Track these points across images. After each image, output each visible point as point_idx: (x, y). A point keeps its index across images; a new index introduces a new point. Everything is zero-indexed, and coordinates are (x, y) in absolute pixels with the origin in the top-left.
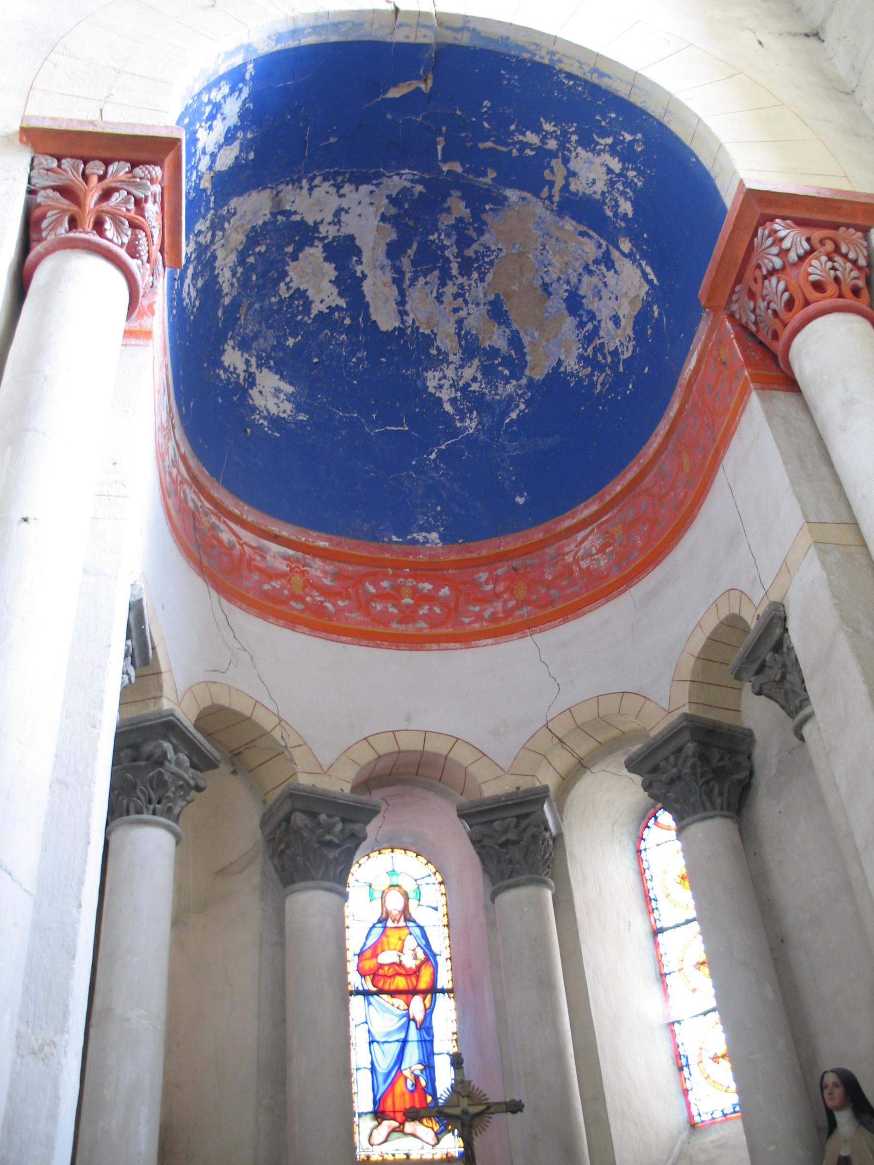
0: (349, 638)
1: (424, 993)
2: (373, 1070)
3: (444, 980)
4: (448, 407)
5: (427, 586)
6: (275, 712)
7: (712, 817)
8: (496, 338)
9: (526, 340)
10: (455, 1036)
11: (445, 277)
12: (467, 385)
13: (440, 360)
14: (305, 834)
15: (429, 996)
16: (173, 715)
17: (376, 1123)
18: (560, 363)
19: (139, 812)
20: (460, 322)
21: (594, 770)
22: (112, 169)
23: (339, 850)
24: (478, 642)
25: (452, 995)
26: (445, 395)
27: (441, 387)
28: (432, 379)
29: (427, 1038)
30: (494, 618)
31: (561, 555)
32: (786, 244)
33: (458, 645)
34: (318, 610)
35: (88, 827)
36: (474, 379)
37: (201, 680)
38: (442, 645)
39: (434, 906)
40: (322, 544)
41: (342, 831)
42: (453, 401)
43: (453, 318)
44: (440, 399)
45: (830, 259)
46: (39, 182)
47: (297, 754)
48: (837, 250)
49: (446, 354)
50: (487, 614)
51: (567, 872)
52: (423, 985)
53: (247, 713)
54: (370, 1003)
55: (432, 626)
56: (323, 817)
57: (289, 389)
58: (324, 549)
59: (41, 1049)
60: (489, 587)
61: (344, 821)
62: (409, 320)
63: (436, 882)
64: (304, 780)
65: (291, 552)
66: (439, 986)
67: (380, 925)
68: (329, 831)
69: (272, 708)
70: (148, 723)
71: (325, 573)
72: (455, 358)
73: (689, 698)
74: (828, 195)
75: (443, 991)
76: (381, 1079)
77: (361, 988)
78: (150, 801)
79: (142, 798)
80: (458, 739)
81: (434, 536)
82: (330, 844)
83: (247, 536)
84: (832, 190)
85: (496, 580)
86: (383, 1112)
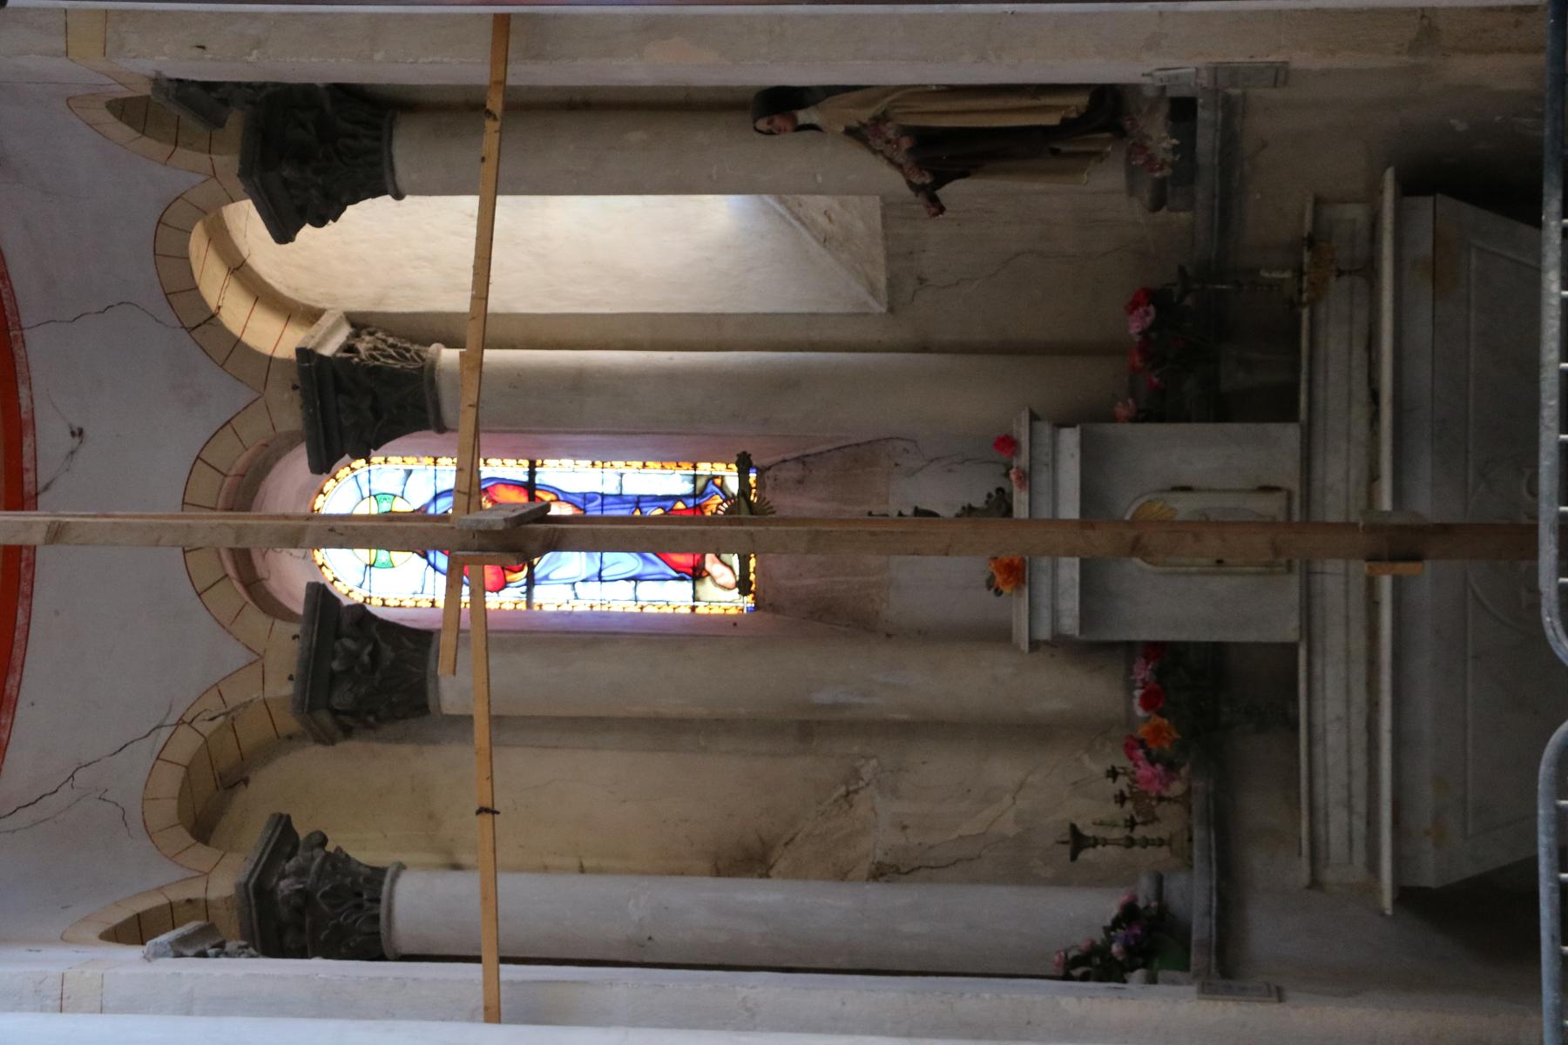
0: (20, 611)
2: (636, 579)
6: (170, 730)
7: (391, 157)
10: (598, 463)
14: (363, 690)
15: (538, 494)
16: (246, 884)
17: (708, 579)
19: (376, 918)
21: (245, 254)
23: (383, 645)
24: (23, 410)
25: (539, 462)
29: (599, 501)
33: (27, 441)
35: (524, 982)
37: (149, 842)
38: (27, 463)
39: (403, 474)
41: (355, 639)
47: (235, 697)
51: (404, 315)
53: (180, 773)
54: (546, 578)
56: (335, 665)
59: (747, 1010)
61: (338, 637)
63: (367, 468)
64: (282, 689)
66: (525, 478)
67: (431, 556)
68: (353, 656)
69: (165, 733)
70: (254, 915)
73: (201, 151)
75: (532, 474)
76: (650, 569)
77: (524, 589)
78: (359, 907)
79: (354, 917)
80: (198, 457)
82: (374, 655)
86: (694, 568)
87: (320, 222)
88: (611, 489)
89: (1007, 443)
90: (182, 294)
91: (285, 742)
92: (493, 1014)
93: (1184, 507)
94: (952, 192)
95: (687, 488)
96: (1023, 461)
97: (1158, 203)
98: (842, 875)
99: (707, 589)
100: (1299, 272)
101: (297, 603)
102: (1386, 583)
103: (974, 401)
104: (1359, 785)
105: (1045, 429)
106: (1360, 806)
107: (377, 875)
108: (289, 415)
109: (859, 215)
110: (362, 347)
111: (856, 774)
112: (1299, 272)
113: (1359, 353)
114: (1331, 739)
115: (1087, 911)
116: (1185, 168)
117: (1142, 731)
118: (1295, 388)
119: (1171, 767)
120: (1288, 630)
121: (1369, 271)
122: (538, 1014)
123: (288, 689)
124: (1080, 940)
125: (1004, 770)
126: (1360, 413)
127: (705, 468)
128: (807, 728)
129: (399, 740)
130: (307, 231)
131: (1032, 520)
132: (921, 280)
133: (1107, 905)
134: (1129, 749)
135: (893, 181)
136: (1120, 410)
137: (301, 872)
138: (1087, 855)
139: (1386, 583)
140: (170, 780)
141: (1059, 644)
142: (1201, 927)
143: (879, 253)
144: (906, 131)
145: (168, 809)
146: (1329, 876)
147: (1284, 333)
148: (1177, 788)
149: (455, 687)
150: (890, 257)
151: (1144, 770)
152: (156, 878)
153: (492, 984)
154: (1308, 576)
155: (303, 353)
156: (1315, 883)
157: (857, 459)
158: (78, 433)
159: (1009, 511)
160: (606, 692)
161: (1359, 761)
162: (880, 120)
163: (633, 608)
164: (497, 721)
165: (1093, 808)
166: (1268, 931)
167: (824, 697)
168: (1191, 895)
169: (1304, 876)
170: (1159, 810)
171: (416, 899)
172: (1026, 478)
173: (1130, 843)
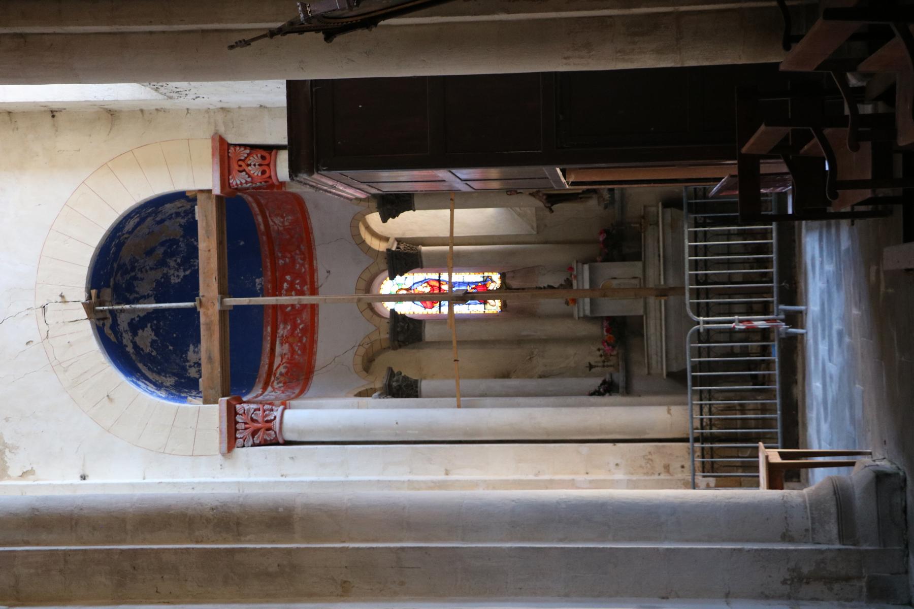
1: (440, 284)
3: (435, 276)
4: (188, 273)
5: (285, 285)
8: (160, 251)
9: (164, 239)
11: (135, 278)
12: (178, 264)
13: (166, 277)
18: (180, 225)
20: (151, 269)
22: (240, 421)
26: (182, 274)
27: (178, 276)
28: (174, 280)
30: (304, 259)
31: (278, 232)
32: (244, 181)
34: (304, 331)
36: (175, 261)
40: (269, 329)
42: (185, 270)
43: (149, 272)
44: (185, 276)
45: (250, 165)
46: (251, 442)
48: (243, 161)
49: (164, 274)
50: (301, 262)
52: (437, 285)
55: (306, 283)
57: (192, 347)
58: (272, 328)
60: (287, 260)
62: (151, 292)
65: (278, 343)
71: (284, 328)
72: (165, 270)
74: (217, 160)
81: (257, 280)
83: (277, 361)
84: (213, 155)
85: (284, 257)
87: (394, 217)
88: (461, 280)
89: (571, 269)
90: (357, 236)
91: (384, 350)
92: (459, 407)
93: (615, 282)
94: (555, 207)
95: (482, 279)
96: (575, 273)
97: (606, 207)
98: (531, 377)
99: (488, 306)
100: (641, 225)
101: (388, 315)
102: (663, 301)
103: (561, 256)
104: (659, 350)
105: (580, 264)
106: (659, 354)
107: (416, 382)
108: (383, 264)
109: (530, 211)
110: (402, 247)
111: (532, 353)
112: (641, 225)
113: (656, 244)
114: (652, 338)
115: (595, 382)
116: (612, 201)
117: (606, 338)
118: (640, 253)
119: (613, 347)
120: (641, 312)
121: (657, 224)
122: (467, 406)
123: (388, 336)
124: (592, 389)
125: (570, 351)
126: (657, 258)
127: (486, 274)
128: (519, 341)
129: (414, 348)
130: (391, 220)
131: (578, 289)
132: (546, 226)
133: (599, 381)
134: (603, 343)
135: (541, 204)
136: (598, 259)
137: (397, 381)
138: (593, 370)
139: (663, 301)
140: (359, 360)
141: (586, 318)
142: (622, 384)
143: (534, 219)
144: (544, 194)
145: (360, 367)
146: (652, 372)
147: (638, 238)
148: (615, 353)
149: (429, 333)
150: (537, 220)
151: (607, 348)
152: (363, 385)
153: (458, 401)
154: (645, 299)
155: (388, 250)
156: (649, 374)
157: (529, 271)
158: (328, 272)
159: (571, 285)
160: (471, 336)
161: (659, 344)
162: (538, 192)
163: (468, 312)
164: (459, 342)
165: (594, 358)
166: (637, 384)
167: (524, 333)
168: (619, 378)
169: (646, 371)
170: (611, 358)
171: (425, 385)
172: (576, 277)
173: (604, 366)
